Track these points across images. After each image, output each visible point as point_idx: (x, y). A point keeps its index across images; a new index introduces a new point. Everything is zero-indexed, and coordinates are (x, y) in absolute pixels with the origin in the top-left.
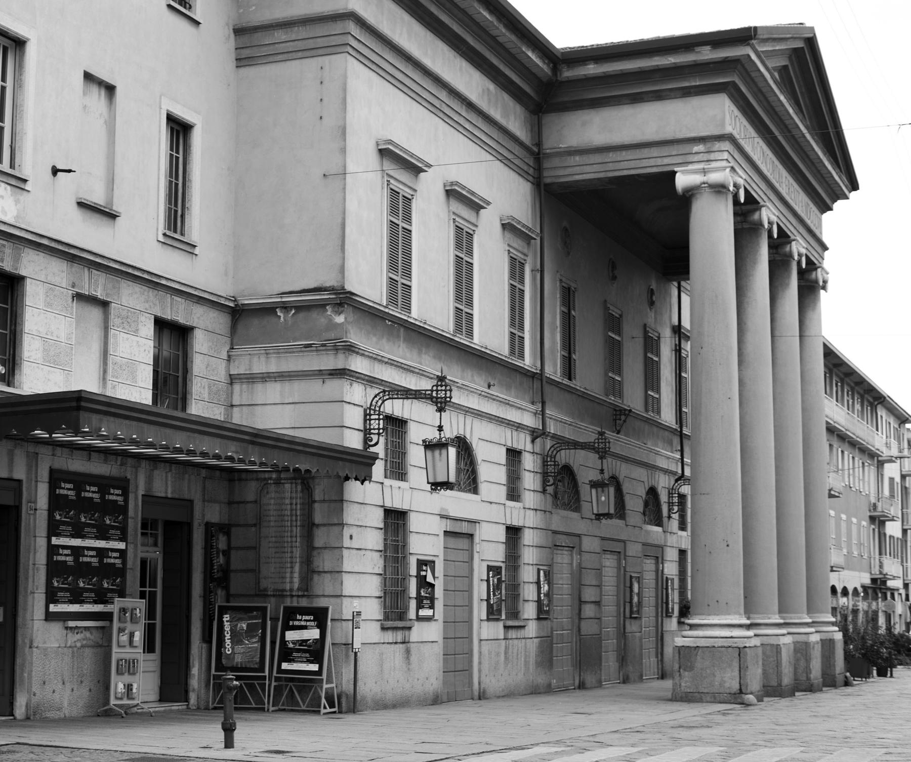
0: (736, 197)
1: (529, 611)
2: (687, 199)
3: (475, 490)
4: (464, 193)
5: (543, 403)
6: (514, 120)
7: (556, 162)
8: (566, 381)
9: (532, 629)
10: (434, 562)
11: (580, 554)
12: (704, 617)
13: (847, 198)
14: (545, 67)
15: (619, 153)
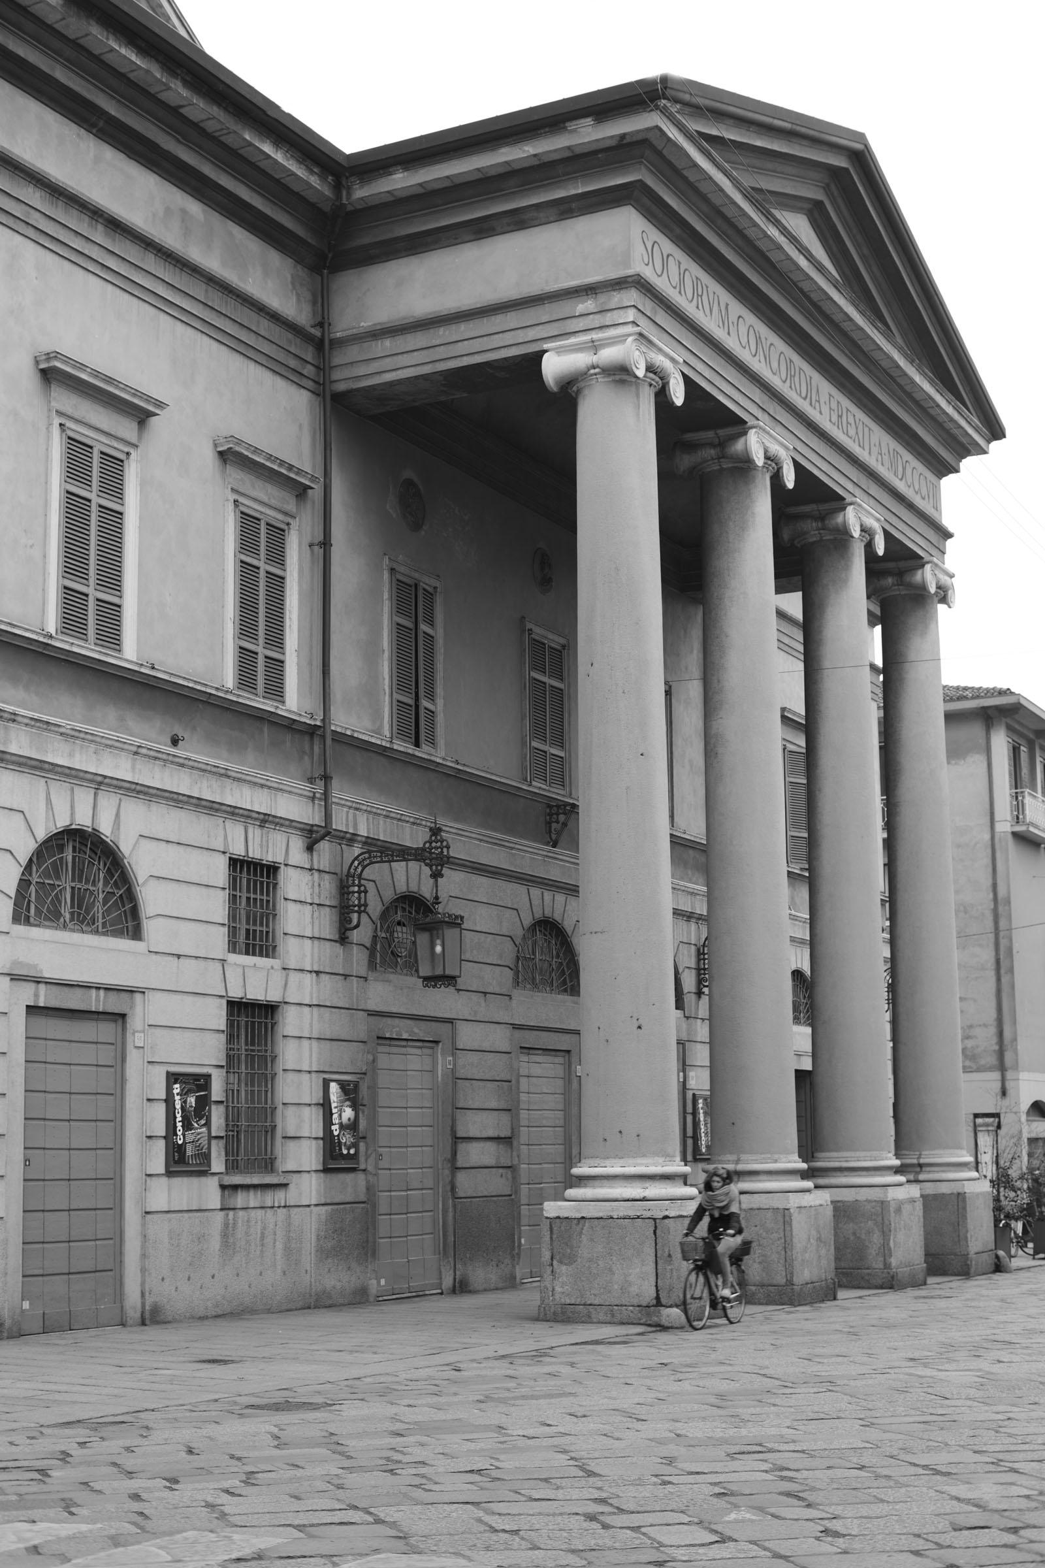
0: (662, 396)
1: (301, 1156)
2: (568, 396)
3: (136, 933)
4: (84, 376)
5: (326, 778)
6: (268, 279)
7: (353, 353)
8: (410, 749)
9: (309, 1188)
10: (210, 1076)
11: (453, 1055)
12: (597, 1161)
13: (985, 452)
14: (314, 181)
15: (454, 327)
